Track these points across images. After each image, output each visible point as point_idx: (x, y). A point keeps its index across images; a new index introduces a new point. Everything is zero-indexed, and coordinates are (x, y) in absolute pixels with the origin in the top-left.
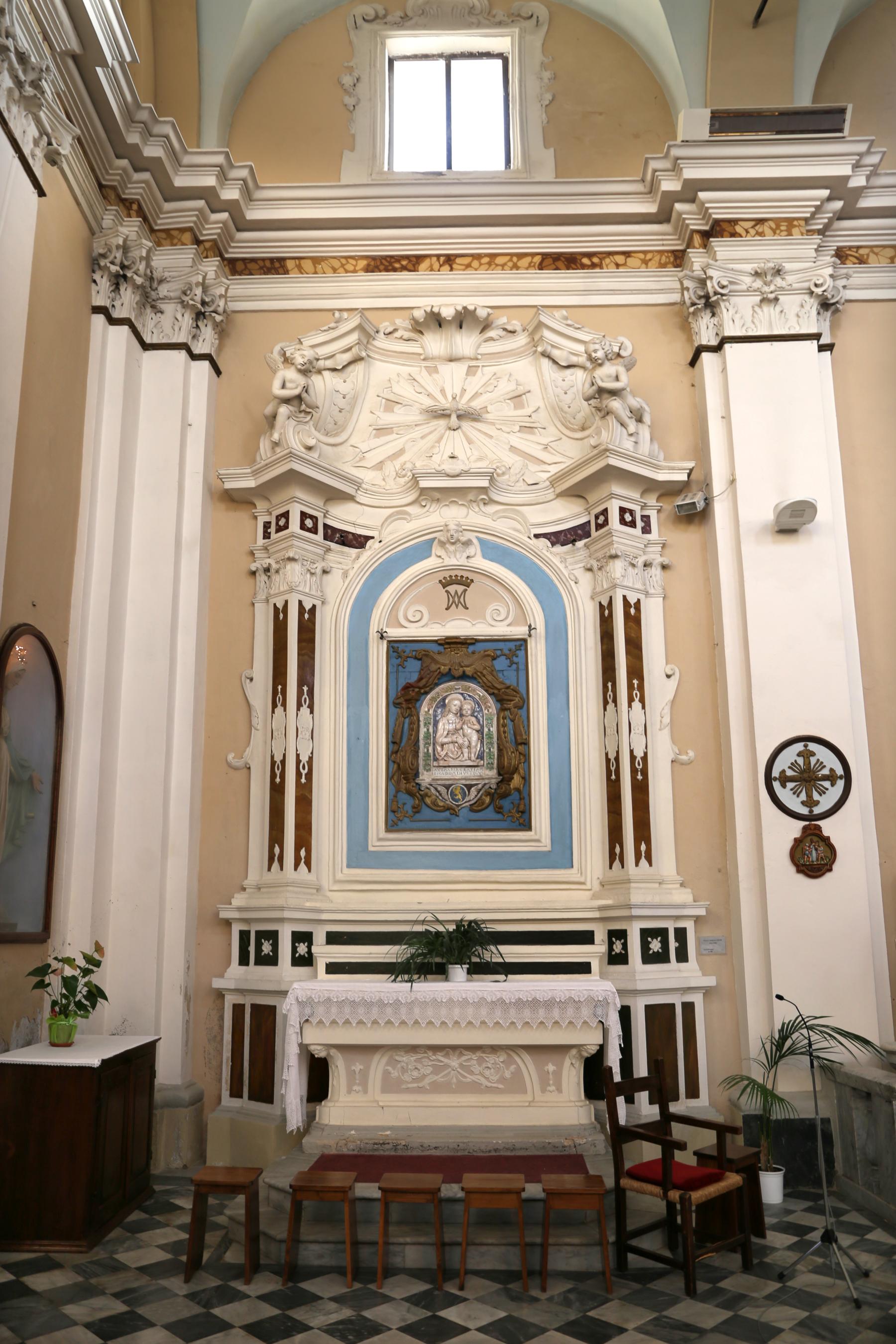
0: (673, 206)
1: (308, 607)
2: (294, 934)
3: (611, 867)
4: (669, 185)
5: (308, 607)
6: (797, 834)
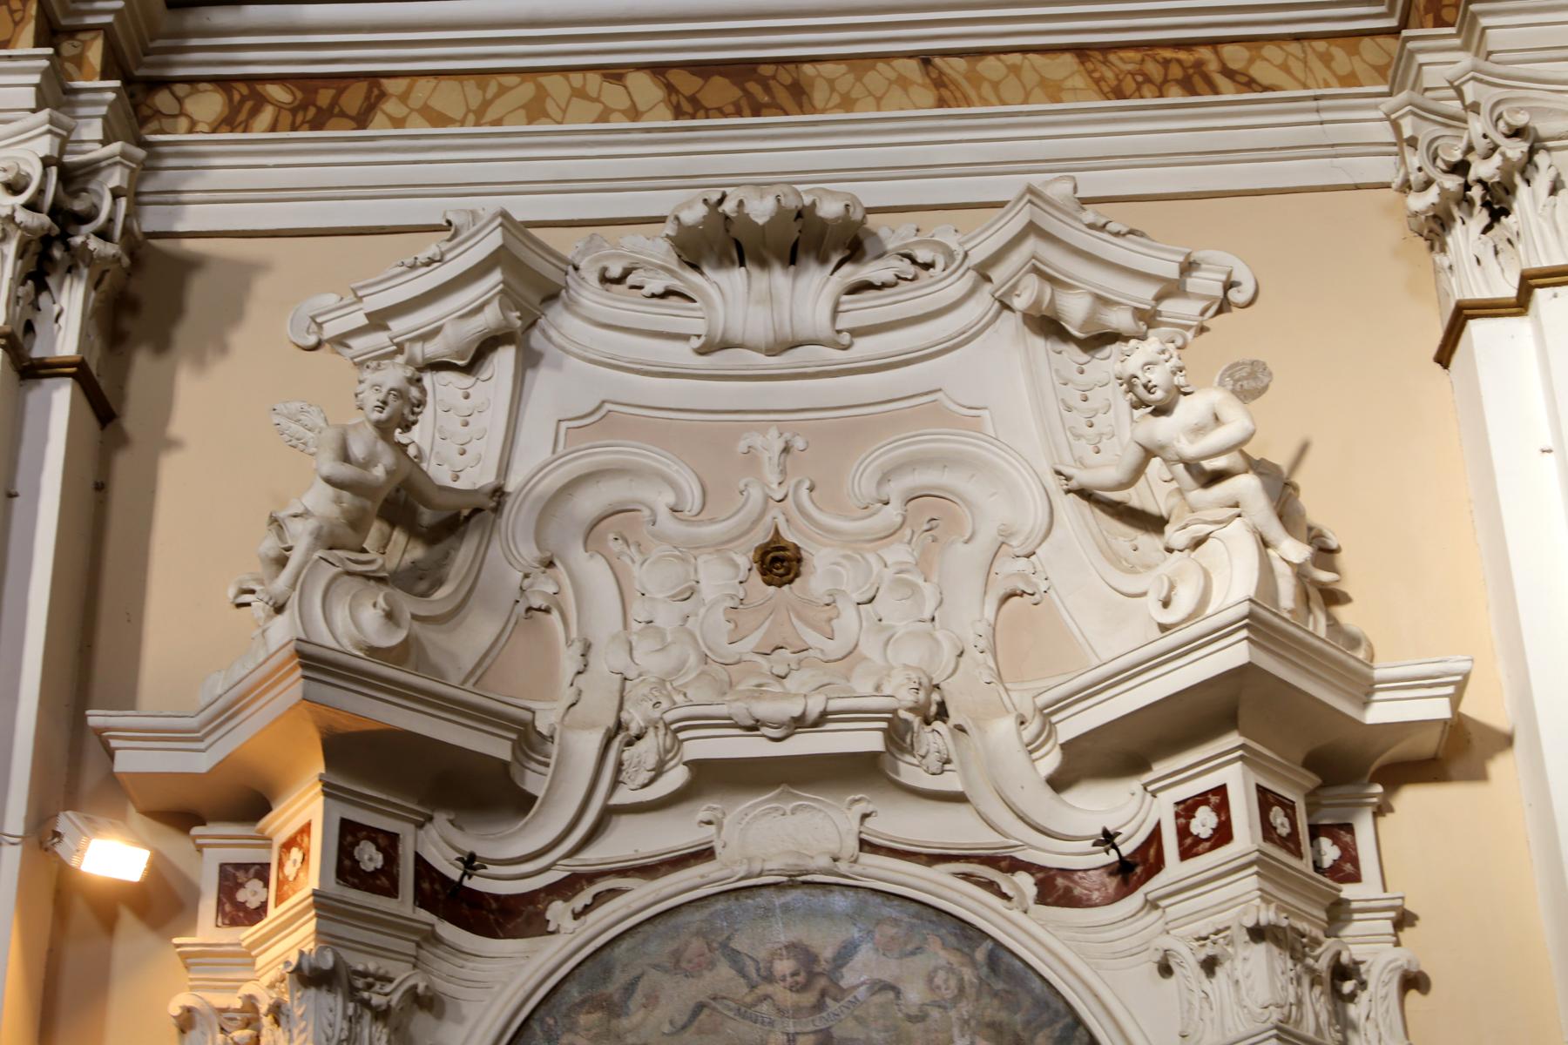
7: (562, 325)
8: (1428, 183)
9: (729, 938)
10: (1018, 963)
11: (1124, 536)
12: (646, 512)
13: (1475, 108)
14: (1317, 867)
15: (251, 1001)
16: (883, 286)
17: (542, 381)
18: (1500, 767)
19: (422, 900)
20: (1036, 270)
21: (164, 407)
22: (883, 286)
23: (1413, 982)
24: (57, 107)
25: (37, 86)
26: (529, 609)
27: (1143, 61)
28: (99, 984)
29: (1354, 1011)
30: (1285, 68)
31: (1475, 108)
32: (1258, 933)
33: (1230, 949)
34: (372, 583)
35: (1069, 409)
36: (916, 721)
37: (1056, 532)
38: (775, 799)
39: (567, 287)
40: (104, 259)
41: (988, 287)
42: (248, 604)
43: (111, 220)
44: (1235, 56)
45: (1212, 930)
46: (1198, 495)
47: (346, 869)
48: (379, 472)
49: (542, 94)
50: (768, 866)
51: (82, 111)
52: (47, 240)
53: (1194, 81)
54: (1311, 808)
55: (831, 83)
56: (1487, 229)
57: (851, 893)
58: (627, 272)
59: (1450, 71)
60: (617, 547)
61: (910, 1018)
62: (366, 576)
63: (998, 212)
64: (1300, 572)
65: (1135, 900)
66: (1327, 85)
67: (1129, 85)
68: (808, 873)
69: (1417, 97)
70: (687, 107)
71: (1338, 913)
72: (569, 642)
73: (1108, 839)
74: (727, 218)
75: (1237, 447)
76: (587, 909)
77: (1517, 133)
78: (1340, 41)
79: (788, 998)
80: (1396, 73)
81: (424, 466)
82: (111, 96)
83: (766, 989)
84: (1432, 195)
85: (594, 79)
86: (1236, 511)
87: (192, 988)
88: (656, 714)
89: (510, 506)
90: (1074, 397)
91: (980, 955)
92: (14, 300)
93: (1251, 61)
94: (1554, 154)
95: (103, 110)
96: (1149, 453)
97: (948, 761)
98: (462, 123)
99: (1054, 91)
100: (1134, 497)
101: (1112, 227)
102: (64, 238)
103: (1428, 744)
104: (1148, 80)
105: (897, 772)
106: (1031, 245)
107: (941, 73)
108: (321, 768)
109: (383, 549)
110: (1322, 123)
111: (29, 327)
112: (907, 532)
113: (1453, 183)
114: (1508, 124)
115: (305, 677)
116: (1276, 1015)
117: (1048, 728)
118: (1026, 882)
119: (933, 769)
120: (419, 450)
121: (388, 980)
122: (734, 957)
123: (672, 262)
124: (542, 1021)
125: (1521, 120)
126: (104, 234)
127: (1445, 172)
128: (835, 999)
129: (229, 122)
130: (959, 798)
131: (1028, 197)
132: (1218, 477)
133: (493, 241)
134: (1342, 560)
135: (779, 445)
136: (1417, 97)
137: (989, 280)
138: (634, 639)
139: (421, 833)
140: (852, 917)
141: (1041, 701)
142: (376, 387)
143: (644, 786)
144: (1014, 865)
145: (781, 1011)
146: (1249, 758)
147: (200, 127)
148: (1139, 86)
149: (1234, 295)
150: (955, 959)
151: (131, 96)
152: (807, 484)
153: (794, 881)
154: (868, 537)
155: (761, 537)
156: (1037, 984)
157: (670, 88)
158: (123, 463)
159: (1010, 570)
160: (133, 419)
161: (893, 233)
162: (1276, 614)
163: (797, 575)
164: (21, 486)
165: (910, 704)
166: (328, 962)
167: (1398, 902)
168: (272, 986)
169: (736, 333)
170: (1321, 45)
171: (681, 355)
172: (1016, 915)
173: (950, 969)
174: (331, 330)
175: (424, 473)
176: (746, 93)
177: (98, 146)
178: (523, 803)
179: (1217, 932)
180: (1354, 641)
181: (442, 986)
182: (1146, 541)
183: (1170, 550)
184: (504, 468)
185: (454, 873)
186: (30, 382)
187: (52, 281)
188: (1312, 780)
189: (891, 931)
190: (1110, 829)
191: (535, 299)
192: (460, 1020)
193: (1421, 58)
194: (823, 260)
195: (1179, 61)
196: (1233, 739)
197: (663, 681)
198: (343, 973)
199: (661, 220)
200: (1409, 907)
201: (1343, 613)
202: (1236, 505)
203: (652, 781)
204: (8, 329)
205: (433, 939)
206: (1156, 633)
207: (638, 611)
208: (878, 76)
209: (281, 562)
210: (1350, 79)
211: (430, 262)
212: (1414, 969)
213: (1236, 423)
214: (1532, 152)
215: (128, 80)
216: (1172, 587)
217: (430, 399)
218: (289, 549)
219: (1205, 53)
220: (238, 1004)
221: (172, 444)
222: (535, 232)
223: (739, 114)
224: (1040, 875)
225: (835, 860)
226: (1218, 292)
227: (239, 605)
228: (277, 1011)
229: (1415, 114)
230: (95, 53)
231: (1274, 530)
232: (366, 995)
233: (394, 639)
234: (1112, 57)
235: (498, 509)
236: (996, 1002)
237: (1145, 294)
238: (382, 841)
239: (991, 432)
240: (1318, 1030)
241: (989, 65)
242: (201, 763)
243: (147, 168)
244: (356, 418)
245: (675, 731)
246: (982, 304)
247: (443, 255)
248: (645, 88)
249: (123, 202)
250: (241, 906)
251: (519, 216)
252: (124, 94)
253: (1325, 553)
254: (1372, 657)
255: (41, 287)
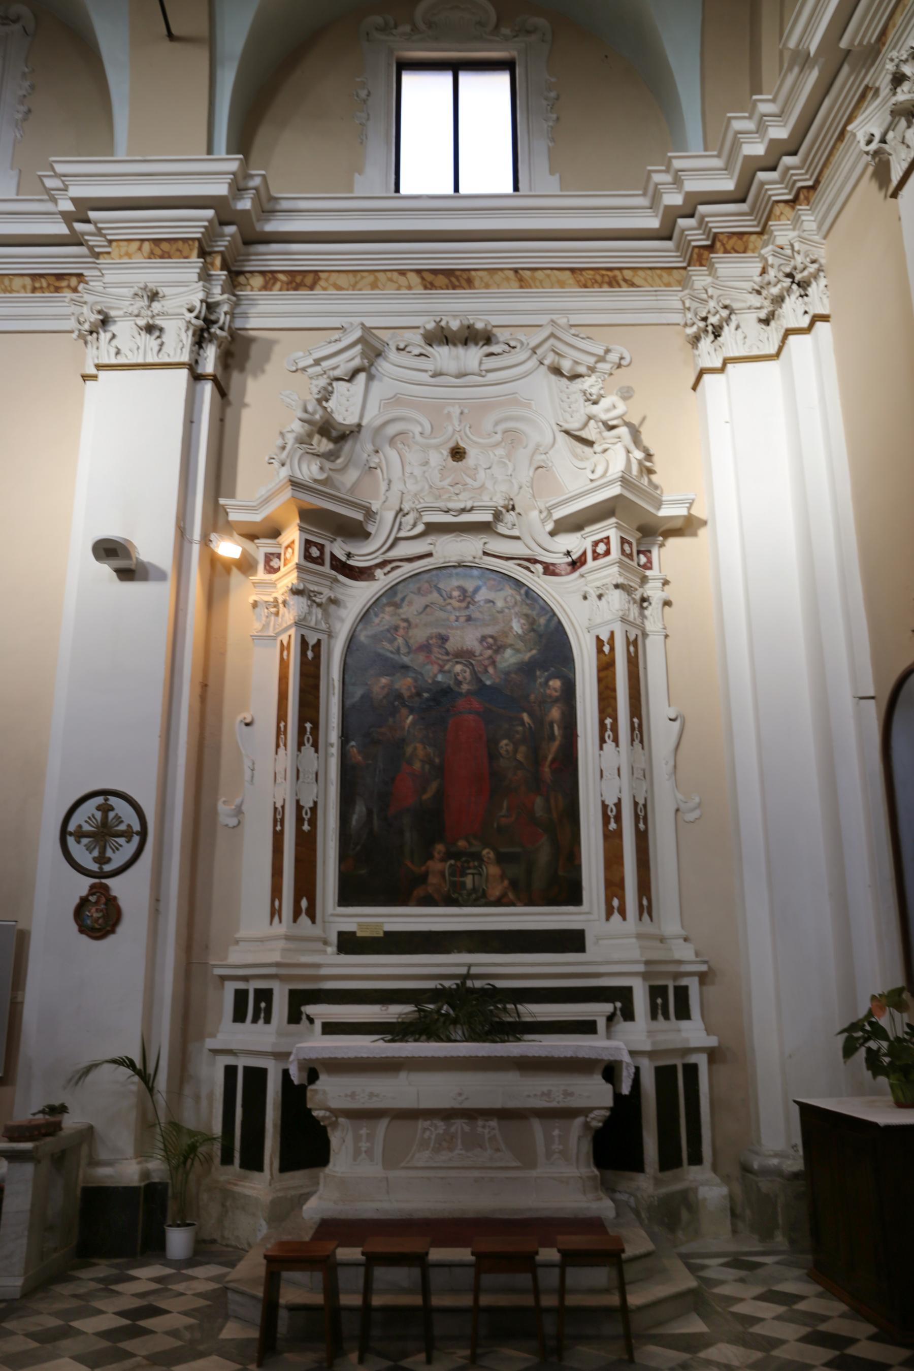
0: (675, 222)
1: (312, 641)
2: (292, 993)
3: (640, 919)
4: (675, 199)
5: (312, 641)
6: (84, 892)
7: (383, 366)
8: (693, 324)
9: (437, 584)
10: (536, 595)
11: (579, 447)
12: (411, 434)
13: (711, 297)
14: (639, 565)
15: (276, 600)
16: (499, 354)
17: (375, 385)
18: (702, 532)
19: (333, 567)
20: (553, 351)
21: (243, 392)
22: (499, 354)
23: (667, 603)
24: (205, 281)
25: (198, 273)
26: (370, 468)
27: (594, 275)
28: (226, 591)
29: (647, 612)
30: (645, 280)
31: (711, 297)
32: (617, 586)
33: (607, 591)
34: (315, 457)
35: (562, 401)
36: (504, 511)
37: (556, 446)
38: (455, 537)
39: (384, 351)
40: (222, 337)
41: (535, 356)
42: (272, 463)
43: (224, 323)
44: (628, 274)
45: (601, 584)
46: (607, 434)
47: (307, 556)
48: (317, 417)
49: (377, 279)
50: (452, 559)
51: (214, 283)
52: (202, 330)
53: (613, 283)
54: (638, 544)
55: (481, 278)
56: (713, 341)
57: (479, 569)
58: (406, 346)
59: (703, 283)
60: (400, 446)
61: (498, 612)
62: (313, 454)
63: (540, 328)
64: (640, 463)
65: (576, 574)
66: (660, 286)
67: (589, 283)
68: (465, 562)
69: (691, 292)
70: (429, 286)
71: (644, 580)
72: (384, 479)
73: (568, 553)
74: (442, 328)
75: (620, 417)
76: (389, 572)
77: (726, 307)
78: (666, 270)
79: (457, 604)
80: (684, 283)
81: (333, 415)
82: (224, 277)
83: (449, 601)
84: (694, 329)
85: (395, 274)
86: (619, 440)
87: (257, 594)
88: (413, 506)
89: (363, 431)
90: (564, 397)
91: (523, 591)
92: (192, 352)
93: (634, 276)
94: (739, 316)
95: (221, 282)
96: (590, 418)
97: (514, 525)
98: (347, 290)
99: (562, 284)
100: (584, 434)
101: (581, 335)
102: (208, 329)
103: (678, 524)
104: (596, 282)
105: (496, 528)
106: (552, 341)
107: (521, 276)
108: (297, 521)
109: (319, 443)
110: (657, 300)
111: (197, 362)
112: (503, 444)
113: (702, 324)
114: (700, 317)
115: (292, 489)
116: (621, 613)
117: (550, 514)
118: (539, 567)
119: (510, 528)
120: (332, 409)
121: (321, 593)
122: (439, 590)
123: (422, 343)
124: (373, 609)
125: (727, 302)
126: (222, 328)
127: (700, 320)
128: (473, 605)
129: (265, 287)
130: (518, 538)
131: (552, 323)
132: (613, 428)
133: (358, 334)
134: (655, 459)
135: (458, 411)
136: (691, 292)
137: (535, 353)
138: (406, 479)
139: (332, 545)
140: (479, 578)
141: (548, 505)
142: (316, 386)
143: (409, 531)
144: (536, 561)
145: (454, 609)
146: (618, 527)
147: (256, 289)
148: (593, 283)
149: (624, 363)
150: (514, 592)
151: (231, 277)
152: (468, 426)
153: (460, 565)
154: (392, 377)
155: (452, 444)
156: (541, 602)
157: (423, 279)
158: (229, 412)
159: (539, 458)
160: (232, 396)
161: (502, 335)
162: (631, 477)
163: (464, 458)
164: (195, 419)
165: (502, 505)
166: (301, 587)
167: (664, 577)
168: (283, 594)
169: (445, 370)
170: (659, 272)
171: (425, 377)
172: (536, 578)
173: (512, 596)
174: (301, 365)
175: (333, 417)
176: (451, 281)
177: (219, 296)
178: (367, 535)
179: (603, 585)
180: (656, 487)
181: (340, 597)
182: (587, 449)
183: (595, 453)
184: (362, 416)
185: (343, 559)
186: (197, 382)
187: (204, 345)
188: (639, 535)
189: (492, 582)
190: (569, 550)
191: (372, 355)
192: (345, 608)
193: (694, 278)
194: (476, 344)
195: (608, 275)
196: (613, 520)
197: (416, 495)
198: (306, 592)
199: (418, 328)
200: (668, 579)
201: (654, 478)
202: (619, 438)
203: (412, 529)
204: (190, 362)
205: (336, 580)
206: (589, 482)
207: (408, 469)
208: (499, 276)
209: (284, 448)
210: (668, 285)
211: (336, 340)
212: (667, 599)
213: (621, 408)
214: (730, 314)
215: (230, 271)
216: (595, 466)
217: (335, 391)
218: (286, 444)
219: (617, 273)
220: (272, 600)
221: (245, 405)
222: (373, 331)
223: (448, 289)
224: (544, 565)
225: (474, 558)
226: (617, 361)
227: (270, 463)
228: (285, 603)
229: (690, 298)
230: (218, 261)
231: (632, 447)
232: (314, 598)
233: (322, 477)
234: (584, 273)
235: (359, 432)
236: (527, 607)
237: (591, 360)
238: (319, 547)
239: (534, 409)
240: (635, 619)
241: (539, 274)
242: (257, 517)
243: (236, 304)
244: (309, 397)
245: (420, 512)
246: (533, 362)
247: (340, 338)
248: (414, 278)
249: (228, 317)
250: (271, 567)
251: (368, 325)
252: (229, 278)
253: (649, 456)
254: (662, 492)
255: (201, 347)
